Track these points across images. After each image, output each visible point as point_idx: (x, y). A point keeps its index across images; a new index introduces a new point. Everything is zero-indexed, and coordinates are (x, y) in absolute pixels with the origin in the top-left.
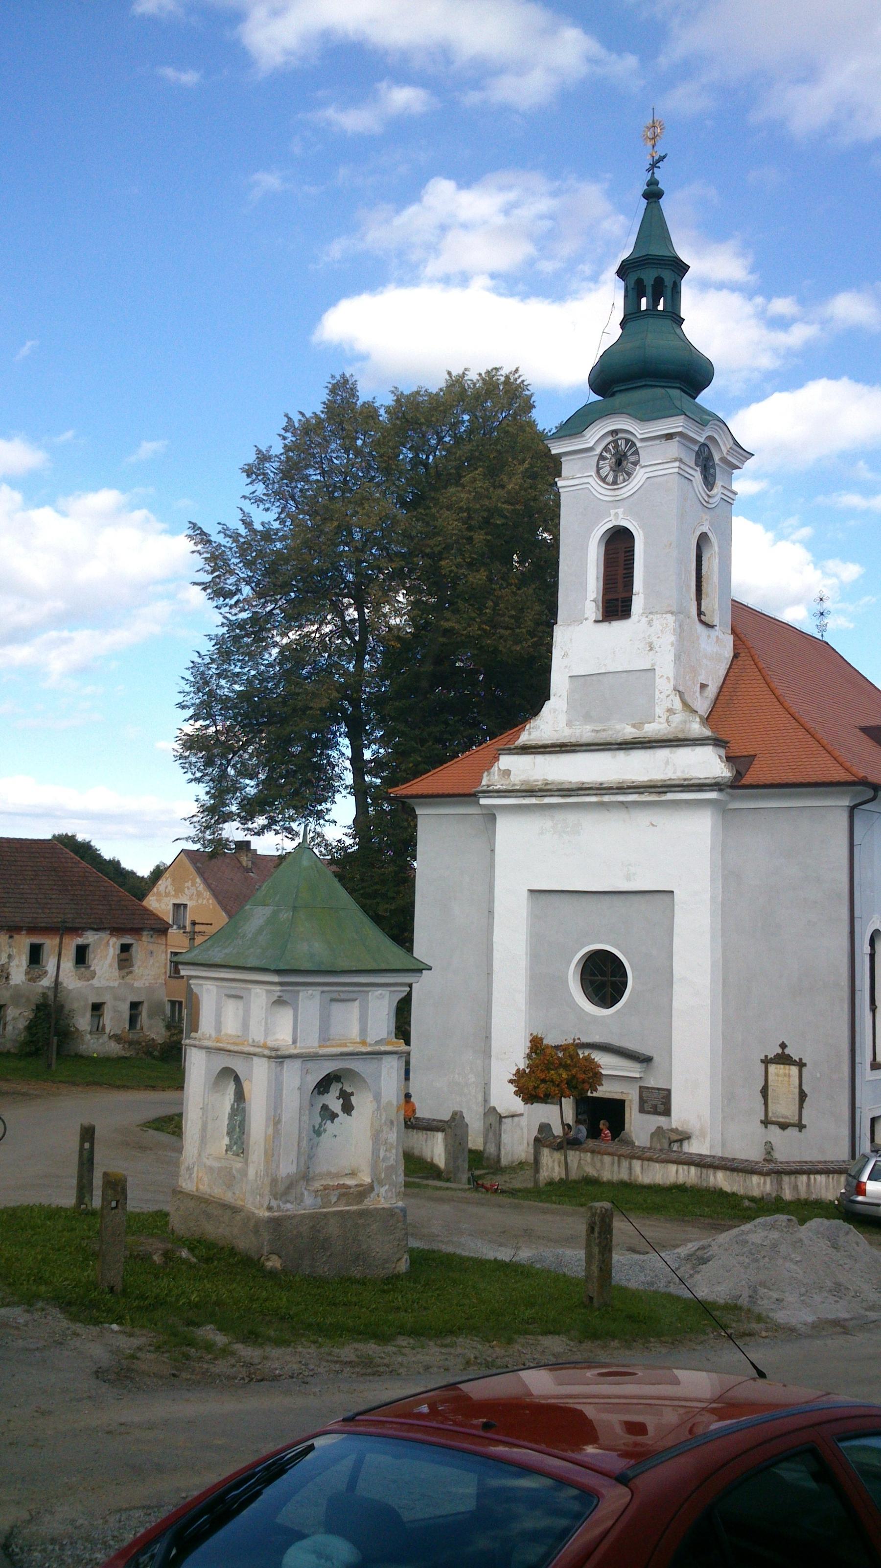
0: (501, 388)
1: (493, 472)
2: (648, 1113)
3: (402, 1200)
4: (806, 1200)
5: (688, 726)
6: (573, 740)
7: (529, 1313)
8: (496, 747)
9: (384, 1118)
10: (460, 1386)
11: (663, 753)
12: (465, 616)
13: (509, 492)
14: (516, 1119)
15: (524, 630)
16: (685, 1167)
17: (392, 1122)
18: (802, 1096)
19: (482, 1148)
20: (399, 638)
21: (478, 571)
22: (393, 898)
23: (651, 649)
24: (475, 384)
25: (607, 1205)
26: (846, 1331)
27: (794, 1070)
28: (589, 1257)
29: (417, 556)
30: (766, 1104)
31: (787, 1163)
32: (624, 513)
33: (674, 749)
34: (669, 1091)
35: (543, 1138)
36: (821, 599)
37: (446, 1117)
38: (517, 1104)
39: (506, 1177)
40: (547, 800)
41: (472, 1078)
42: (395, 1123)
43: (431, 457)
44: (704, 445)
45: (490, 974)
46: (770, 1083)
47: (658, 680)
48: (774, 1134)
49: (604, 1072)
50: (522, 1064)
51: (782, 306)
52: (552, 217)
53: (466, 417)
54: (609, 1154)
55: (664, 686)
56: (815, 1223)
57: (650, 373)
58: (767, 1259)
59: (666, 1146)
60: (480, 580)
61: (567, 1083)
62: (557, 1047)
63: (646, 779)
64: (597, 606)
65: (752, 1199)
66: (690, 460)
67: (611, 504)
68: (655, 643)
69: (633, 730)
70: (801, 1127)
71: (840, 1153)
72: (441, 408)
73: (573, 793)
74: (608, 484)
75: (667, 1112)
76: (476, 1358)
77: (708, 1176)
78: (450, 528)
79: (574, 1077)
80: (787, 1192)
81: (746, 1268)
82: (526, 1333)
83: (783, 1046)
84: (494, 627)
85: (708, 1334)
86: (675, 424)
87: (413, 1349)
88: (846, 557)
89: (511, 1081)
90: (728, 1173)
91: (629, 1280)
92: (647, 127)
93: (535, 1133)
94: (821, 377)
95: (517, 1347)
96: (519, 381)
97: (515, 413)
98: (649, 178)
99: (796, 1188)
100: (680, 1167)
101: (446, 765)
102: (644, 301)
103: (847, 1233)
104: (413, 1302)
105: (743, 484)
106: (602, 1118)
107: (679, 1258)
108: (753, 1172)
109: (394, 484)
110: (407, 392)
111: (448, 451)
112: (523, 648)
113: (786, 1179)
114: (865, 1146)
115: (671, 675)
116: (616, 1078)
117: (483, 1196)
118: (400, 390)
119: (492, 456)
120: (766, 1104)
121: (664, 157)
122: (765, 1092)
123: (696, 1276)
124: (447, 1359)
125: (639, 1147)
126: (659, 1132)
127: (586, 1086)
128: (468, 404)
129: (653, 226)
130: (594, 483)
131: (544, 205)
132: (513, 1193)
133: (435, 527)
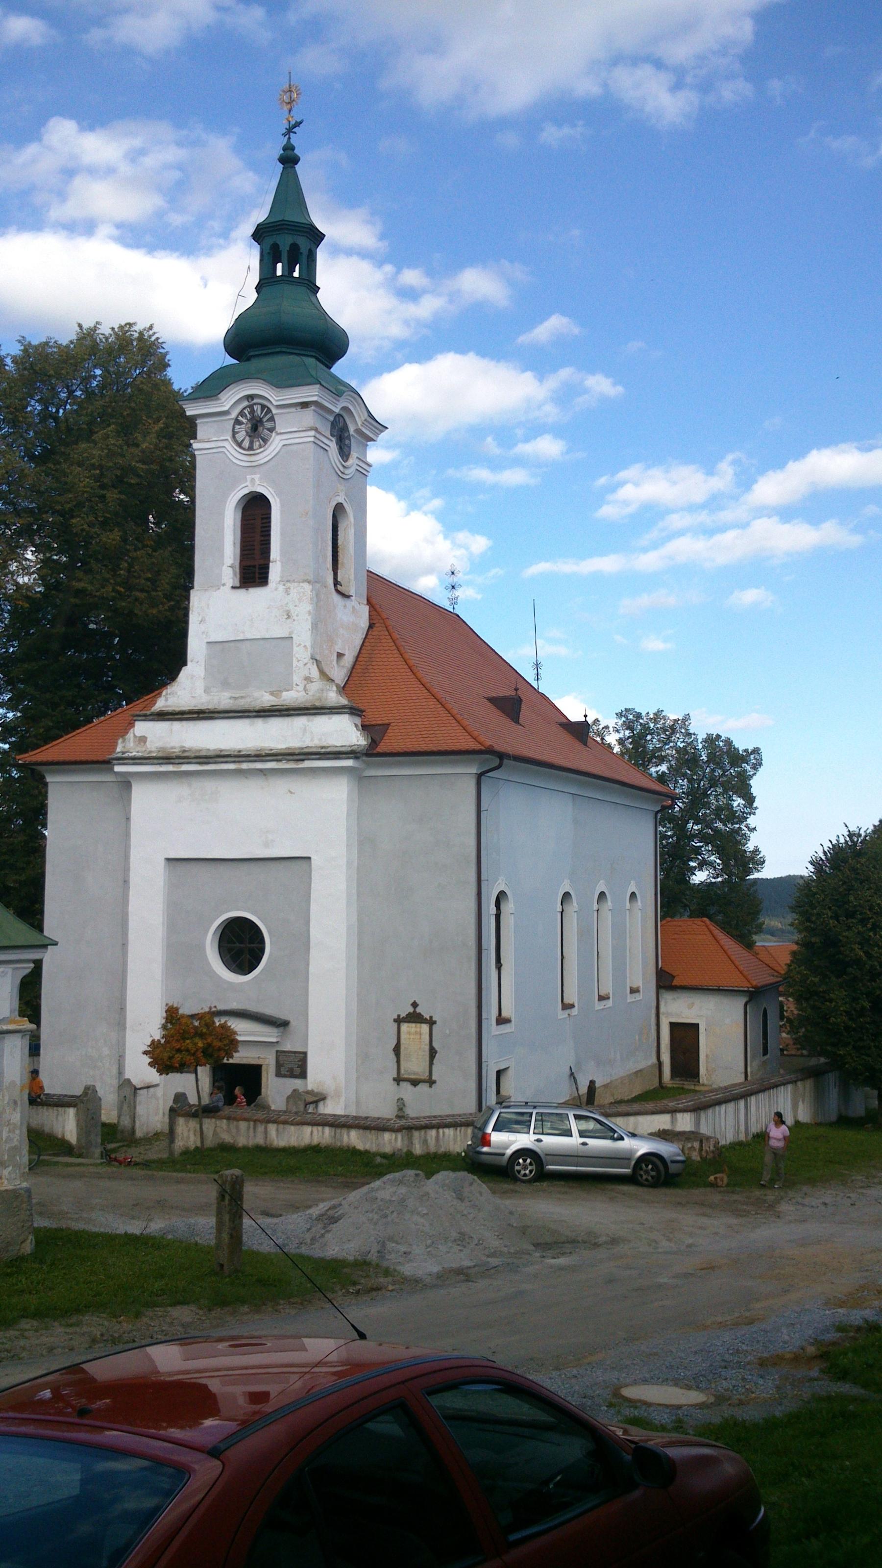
0: (135, 344)
1: (127, 430)
2: (285, 1076)
3: (26, 1180)
4: (217, 1230)
5: (325, 694)
6: (211, 707)
7: (159, 1284)
8: (131, 713)
9: (7, 1098)
10: (83, 1366)
11: (300, 722)
12: (98, 577)
13: (143, 451)
14: (151, 1090)
15: (160, 593)
16: (320, 1128)
17: (15, 1102)
18: (433, 1052)
19: (116, 1121)
20: (27, 598)
21: (111, 531)
22: (23, 869)
23: (289, 617)
24: (107, 339)
25: (237, 1172)
26: (468, 1279)
27: (425, 1028)
28: (220, 1224)
29: (47, 512)
30: (398, 1062)
31: (417, 1118)
32: (260, 479)
33: (311, 717)
34: (305, 1054)
35: (179, 1108)
36: (453, 573)
37: (78, 1091)
38: (153, 1075)
39: (142, 1149)
40: (185, 768)
41: (106, 1051)
42: (19, 1103)
43: (61, 411)
44: (339, 415)
45: (124, 945)
46: (402, 1041)
47: (295, 648)
48: (407, 1091)
49: (239, 1038)
50: (157, 1035)
51: (412, 277)
52: (180, 167)
53: (98, 372)
54: (245, 1120)
55: (301, 653)
56: (443, 1176)
57: (287, 340)
58: (395, 1214)
59: (301, 1107)
60: (113, 540)
61: (203, 1052)
62: (193, 1016)
63: (284, 746)
64: (235, 574)
65: (384, 1156)
66: (326, 430)
67: (248, 470)
68: (292, 611)
69: (272, 698)
70: (431, 1082)
71: (467, 1105)
72: (72, 361)
73: (211, 760)
74: (244, 449)
75: (303, 1075)
76: (102, 1335)
77: (341, 1135)
78: (81, 485)
79: (209, 1045)
80: (417, 1146)
81: (376, 1224)
82: (154, 1305)
83: (415, 1005)
84: (130, 588)
85: (336, 1292)
86: (311, 393)
87: (36, 1331)
88: (475, 530)
89: (145, 1053)
90: (361, 1131)
91: (261, 1244)
92: (284, 91)
93: (170, 1103)
94: (449, 351)
95: (145, 1320)
96: (153, 339)
97: (149, 370)
98: (285, 142)
99: (425, 1141)
100: (315, 1128)
101: (78, 731)
102: (279, 266)
103: (471, 1184)
104: (38, 1283)
105: (376, 454)
106: (240, 1084)
107: (311, 1218)
108: (384, 1129)
109: (21, 436)
110: (35, 342)
111: (80, 405)
112: (159, 612)
113: (416, 1134)
114: (491, 1098)
115: (308, 644)
116: (252, 1042)
117: (114, 1169)
118: (28, 340)
119: (125, 413)
120: (398, 1062)
121: (301, 123)
122: (397, 1050)
123: (326, 1235)
124: (71, 1339)
125: (274, 1111)
126: (295, 1095)
127: (222, 1053)
128: (100, 358)
129: (289, 192)
130: (230, 447)
131: (172, 154)
132: (146, 1165)
133: (66, 483)
